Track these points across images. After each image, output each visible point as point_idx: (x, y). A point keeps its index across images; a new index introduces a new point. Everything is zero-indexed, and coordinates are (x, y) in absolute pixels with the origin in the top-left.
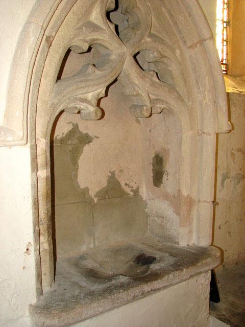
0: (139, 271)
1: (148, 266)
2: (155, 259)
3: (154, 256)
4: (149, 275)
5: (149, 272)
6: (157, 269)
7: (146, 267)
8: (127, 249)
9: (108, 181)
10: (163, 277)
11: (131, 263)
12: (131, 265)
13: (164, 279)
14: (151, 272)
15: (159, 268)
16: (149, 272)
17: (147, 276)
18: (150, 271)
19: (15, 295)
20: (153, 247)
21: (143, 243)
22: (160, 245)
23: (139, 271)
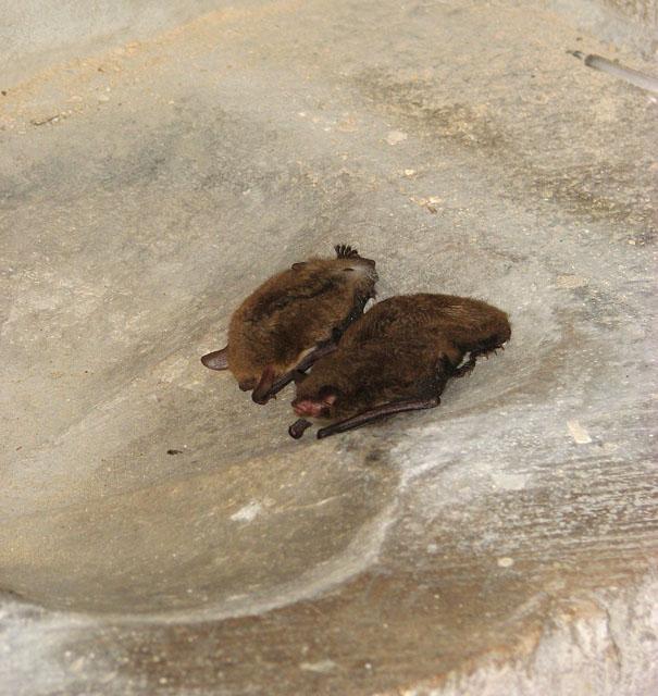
0: (247, 514)
1: (374, 457)
2: (489, 331)
3: (481, 294)
4: (369, 583)
5: (368, 550)
6: (493, 503)
7: (350, 463)
8: (149, 166)
9: (418, 295)
10: (542, 622)
11: (183, 374)
12: (175, 414)
13: (559, 652)
14: (393, 546)
15: (517, 481)
16: (368, 550)
17: (326, 606)
18: (382, 526)
19: (520, 431)
20: (492, 141)
21: (374, 88)
22: (607, 110)
23: (247, 514)
